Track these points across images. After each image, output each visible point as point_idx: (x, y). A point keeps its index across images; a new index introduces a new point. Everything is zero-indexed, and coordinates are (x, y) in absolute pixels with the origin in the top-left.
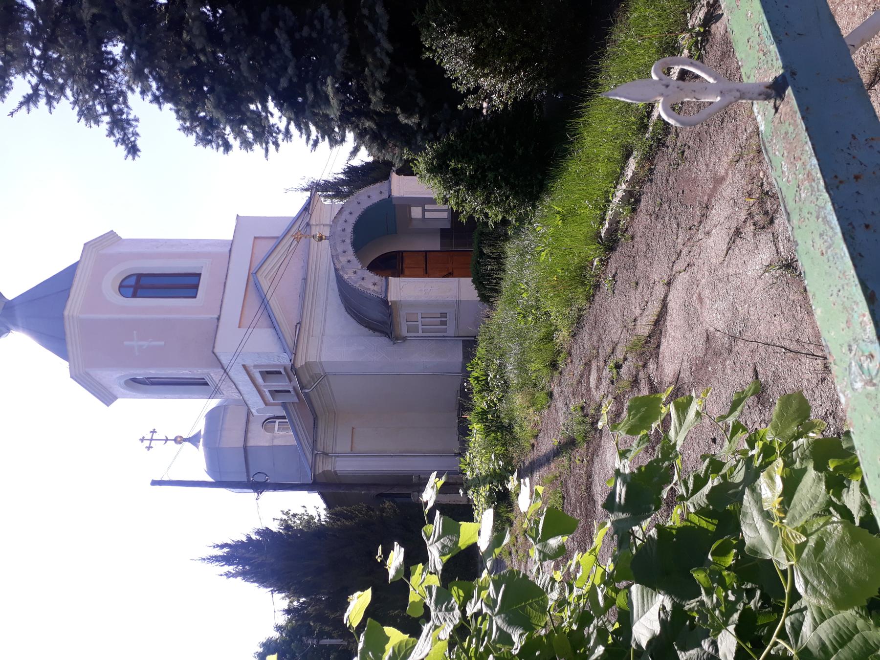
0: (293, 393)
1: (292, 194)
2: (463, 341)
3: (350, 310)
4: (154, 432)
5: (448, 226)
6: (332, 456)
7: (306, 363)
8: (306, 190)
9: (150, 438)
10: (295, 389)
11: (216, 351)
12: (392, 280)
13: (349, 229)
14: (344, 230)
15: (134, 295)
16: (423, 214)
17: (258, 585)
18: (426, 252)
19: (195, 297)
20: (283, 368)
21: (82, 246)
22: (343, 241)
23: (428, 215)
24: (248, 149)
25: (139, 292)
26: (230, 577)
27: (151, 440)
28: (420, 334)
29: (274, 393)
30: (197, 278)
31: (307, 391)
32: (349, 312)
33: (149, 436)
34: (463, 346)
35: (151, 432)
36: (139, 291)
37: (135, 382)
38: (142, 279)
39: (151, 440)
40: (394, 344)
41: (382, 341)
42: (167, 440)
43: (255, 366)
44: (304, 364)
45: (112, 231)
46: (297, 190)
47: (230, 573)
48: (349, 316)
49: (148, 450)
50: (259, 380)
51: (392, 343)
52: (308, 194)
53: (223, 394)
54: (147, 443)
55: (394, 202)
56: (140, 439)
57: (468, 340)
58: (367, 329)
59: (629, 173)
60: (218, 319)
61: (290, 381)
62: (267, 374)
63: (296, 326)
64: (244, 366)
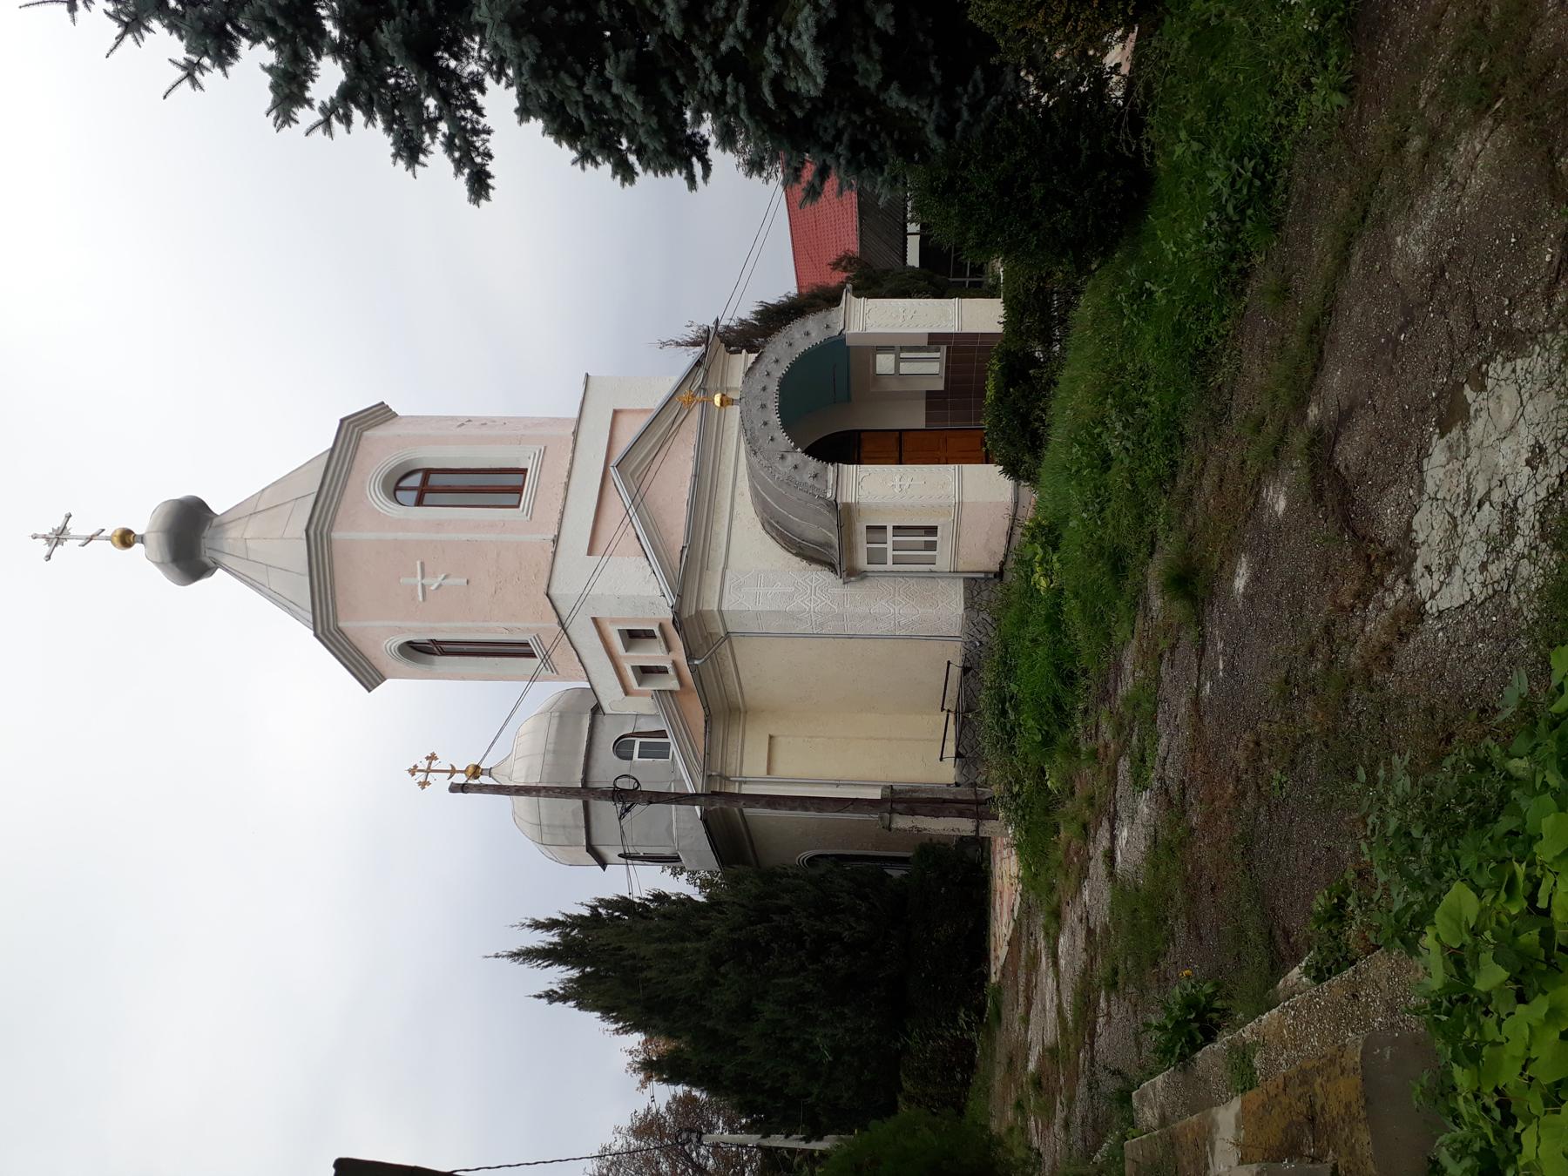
0: (671, 672)
2: (965, 579)
3: (770, 523)
4: (432, 757)
5: (939, 385)
6: (735, 781)
7: (697, 611)
8: (695, 344)
9: (425, 768)
10: (674, 664)
12: (850, 470)
13: (774, 387)
14: (764, 389)
15: (419, 502)
16: (897, 367)
17: (599, 1014)
18: (901, 431)
19: (518, 506)
20: (657, 625)
21: (338, 423)
22: (763, 406)
23: (905, 368)
24: (659, 173)
25: (428, 497)
26: (555, 1001)
27: (428, 771)
28: (890, 566)
29: (644, 672)
31: (696, 662)
32: (768, 529)
33: (424, 765)
35: (427, 758)
37: (415, 648)
39: (428, 771)
40: (844, 583)
41: (821, 576)
43: (613, 621)
44: (693, 613)
45: (383, 403)
46: (678, 344)
47: (556, 992)
48: (767, 537)
49: (423, 788)
51: (841, 581)
52: (699, 350)
53: (558, 673)
54: (420, 777)
56: (410, 771)
57: (973, 579)
59: (1221, 667)
60: (556, 541)
61: (669, 649)
62: (633, 637)
63: (682, 551)
64: (595, 620)
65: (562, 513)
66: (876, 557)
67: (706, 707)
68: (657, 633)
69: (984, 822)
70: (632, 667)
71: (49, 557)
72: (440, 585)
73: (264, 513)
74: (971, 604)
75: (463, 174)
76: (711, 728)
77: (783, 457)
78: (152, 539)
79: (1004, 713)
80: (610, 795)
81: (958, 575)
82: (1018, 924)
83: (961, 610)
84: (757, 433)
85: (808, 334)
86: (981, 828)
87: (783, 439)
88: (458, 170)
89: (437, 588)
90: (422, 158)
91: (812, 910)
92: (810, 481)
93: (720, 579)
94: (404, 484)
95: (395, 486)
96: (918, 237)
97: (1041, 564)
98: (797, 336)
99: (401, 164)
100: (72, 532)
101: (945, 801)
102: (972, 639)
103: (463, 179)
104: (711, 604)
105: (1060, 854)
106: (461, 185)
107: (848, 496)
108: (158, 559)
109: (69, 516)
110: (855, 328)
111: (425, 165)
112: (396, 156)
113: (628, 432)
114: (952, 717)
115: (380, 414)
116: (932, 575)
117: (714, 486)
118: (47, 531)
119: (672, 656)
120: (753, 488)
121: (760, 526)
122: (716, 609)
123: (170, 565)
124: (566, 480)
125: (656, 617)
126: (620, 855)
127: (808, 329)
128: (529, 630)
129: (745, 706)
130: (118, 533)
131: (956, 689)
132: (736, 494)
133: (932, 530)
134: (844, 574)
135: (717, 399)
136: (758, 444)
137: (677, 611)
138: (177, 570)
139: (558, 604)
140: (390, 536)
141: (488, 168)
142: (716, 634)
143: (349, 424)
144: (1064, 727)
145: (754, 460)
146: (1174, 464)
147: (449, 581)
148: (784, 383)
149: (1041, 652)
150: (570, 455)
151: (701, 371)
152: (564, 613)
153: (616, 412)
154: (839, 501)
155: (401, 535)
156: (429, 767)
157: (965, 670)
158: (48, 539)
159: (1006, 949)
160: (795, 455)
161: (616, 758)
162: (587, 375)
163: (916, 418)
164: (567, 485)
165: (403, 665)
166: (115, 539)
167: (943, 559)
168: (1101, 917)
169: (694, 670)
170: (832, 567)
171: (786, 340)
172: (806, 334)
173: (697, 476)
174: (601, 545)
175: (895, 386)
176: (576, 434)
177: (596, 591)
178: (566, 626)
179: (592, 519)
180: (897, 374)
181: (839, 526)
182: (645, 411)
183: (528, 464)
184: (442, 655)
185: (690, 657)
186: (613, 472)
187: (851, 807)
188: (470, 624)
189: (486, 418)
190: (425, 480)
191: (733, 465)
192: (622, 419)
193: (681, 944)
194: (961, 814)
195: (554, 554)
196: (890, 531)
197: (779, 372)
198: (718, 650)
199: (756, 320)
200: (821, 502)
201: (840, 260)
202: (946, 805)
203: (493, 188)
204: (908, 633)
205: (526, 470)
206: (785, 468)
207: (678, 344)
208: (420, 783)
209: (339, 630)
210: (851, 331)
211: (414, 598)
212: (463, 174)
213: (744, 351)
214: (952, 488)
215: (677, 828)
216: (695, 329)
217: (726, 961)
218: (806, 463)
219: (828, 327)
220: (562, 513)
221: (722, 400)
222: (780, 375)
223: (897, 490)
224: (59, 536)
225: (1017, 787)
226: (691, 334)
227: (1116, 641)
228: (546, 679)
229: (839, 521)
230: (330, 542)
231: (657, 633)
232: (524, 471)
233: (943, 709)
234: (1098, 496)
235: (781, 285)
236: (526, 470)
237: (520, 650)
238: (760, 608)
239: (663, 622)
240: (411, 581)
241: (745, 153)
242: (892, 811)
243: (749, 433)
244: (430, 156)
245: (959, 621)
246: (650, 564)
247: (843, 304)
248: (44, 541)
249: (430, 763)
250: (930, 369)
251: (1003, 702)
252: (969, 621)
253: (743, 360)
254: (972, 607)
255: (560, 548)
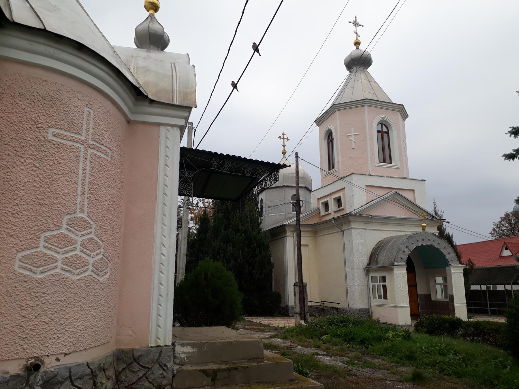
0: (327, 213)
1: (433, 207)
2: (369, 309)
3: (382, 243)
4: (288, 139)
5: (433, 299)
7: (351, 221)
9: (285, 137)
10: (330, 214)
11: (353, 175)
12: (405, 270)
14: (429, 240)
15: (378, 131)
18: (416, 286)
19: (379, 162)
22: (423, 240)
23: (438, 287)
27: (284, 139)
28: (371, 284)
29: (326, 204)
30: (389, 162)
31: (333, 221)
32: (379, 243)
33: (285, 137)
34: (366, 309)
35: (288, 138)
36: (380, 134)
37: (330, 133)
38: (386, 135)
39: (284, 139)
41: (366, 261)
42: (284, 146)
43: (344, 194)
44: (350, 220)
45: (408, 116)
46: (435, 208)
48: (377, 243)
50: (336, 196)
51: (364, 268)
55: (447, 268)
57: (369, 311)
58: (370, 253)
60: (369, 175)
61: (335, 212)
62: (339, 201)
63: (370, 215)
65: (378, 176)
66: (374, 279)
67: (316, 224)
68: (340, 208)
69: (299, 316)
70: (328, 201)
71: (350, 22)
72: (352, 140)
73: (370, 84)
74: (360, 310)
75: (514, 152)
76: (310, 226)
77: (407, 247)
78: (358, 53)
79: (342, 322)
80: (298, 199)
81: (370, 306)
82: (268, 326)
83: (358, 308)
84: (414, 238)
85: (449, 254)
86: (297, 314)
87: (413, 247)
88: (514, 151)
89: (351, 140)
90: (513, 136)
91: (261, 261)
92: (400, 257)
93: (362, 228)
94: (383, 126)
95: (382, 123)
96: (480, 289)
97: (396, 334)
98: (448, 250)
99: (511, 129)
100: (358, 28)
101: (304, 303)
102: (348, 311)
103: (512, 152)
104: (353, 225)
105: (304, 339)
106: (510, 151)
107: (396, 269)
108: (352, 54)
109: (363, 26)
110: (453, 270)
111: (510, 136)
112: (513, 128)
113: (408, 195)
114: (319, 304)
115: (405, 116)
116: (369, 298)
117: (393, 224)
118: (358, 20)
119: (333, 213)
120: (392, 238)
121: (380, 240)
122: (352, 227)
123: (351, 58)
124: (389, 176)
125: (347, 208)
126: (262, 198)
127: (451, 253)
128: (339, 168)
129: (317, 236)
130: (359, 41)
131: (329, 306)
132: (390, 232)
133: (386, 297)
134: (367, 268)
135: (424, 224)
136: (410, 239)
137: (350, 214)
138: (349, 60)
139: (349, 177)
140: (367, 124)
141: (516, 158)
142: (343, 227)
143: (402, 108)
144: (345, 341)
145: (405, 238)
146: (450, 375)
147: (353, 143)
148: (432, 246)
149: (369, 334)
150: (398, 177)
151: (431, 218)
152: (346, 179)
153: (413, 190)
154: (394, 266)
155: (367, 127)
156: (285, 139)
157: (337, 309)
158: (355, 21)
159: (258, 322)
160: (408, 251)
161: (292, 195)
162: (425, 180)
163: (421, 291)
164: (388, 177)
165: (324, 131)
166: (357, 41)
167: (375, 301)
168: (294, 350)
169: (330, 220)
170: (369, 264)
171: (446, 246)
172: (449, 254)
173: (395, 219)
174: (369, 189)
175: (432, 284)
176: (405, 178)
177: (354, 188)
178: (342, 179)
179: (377, 185)
180: (436, 285)
181: (385, 267)
182: (415, 200)
183: (393, 164)
184: (328, 142)
185: (335, 219)
186: (394, 191)
187: (300, 273)
188: (340, 150)
189: (406, 149)
190: (385, 132)
191: (400, 230)
192: (412, 192)
193: (250, 221)
194: (301, 308)
195: (365, 175)
196: (384, 284)
197: (435, 245)
198: (336, 227)
199: (446, 234)
200: (393, 261)
201: (472, 263)
202: (303, 303)
203: (509, 161)
204: (349, 290)
205: (391, 163)
206: (403, 248)
207: (435, 208)
208: (288, 141)
209: (335, 111)
210: (451, 268)
211: (347, 133)
212: (514, 152)
213: (439, 232)
214: (402, 304)
215: (271, 215)
216: (441, 213)
217: (245, 235)
218: (405, 255)
219: (452, 260)
220: (378, 176)
221: (424, 226)
222: (434, 245)
223: (399, 286)
224: (356, 24)
225: (319, 326)
226: (439, 212)
227: (382, 357)
228: (322, 174)
229: (387, 267)
230: (364, 106)
231: (340, 208)
232: (391, 163)
233: (322, 301)
234: (431, 352)
235: (458, 241)
236: (391, 163)
237: (331, 165)
238: (354, 241)
239: (345, 210)
240: (353, 131)
241: (500, 225)
242: (300, 286)
243: (414, 235)
244: (514, 138)
245: (354, 307)
246: (364, 205)
247: (460, 265)
248: (354, 20)
249: (286, 139)
250: (439, 295)
251: (345, 322)
252: (354, 311)
253: (437, 232)
254: (360, 311)
255: (367, 176)
